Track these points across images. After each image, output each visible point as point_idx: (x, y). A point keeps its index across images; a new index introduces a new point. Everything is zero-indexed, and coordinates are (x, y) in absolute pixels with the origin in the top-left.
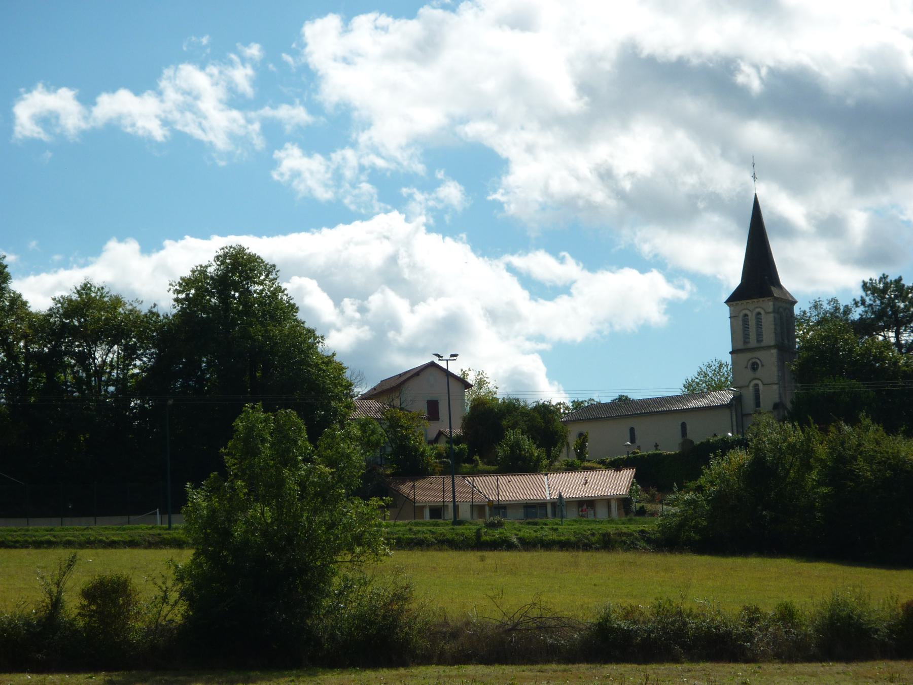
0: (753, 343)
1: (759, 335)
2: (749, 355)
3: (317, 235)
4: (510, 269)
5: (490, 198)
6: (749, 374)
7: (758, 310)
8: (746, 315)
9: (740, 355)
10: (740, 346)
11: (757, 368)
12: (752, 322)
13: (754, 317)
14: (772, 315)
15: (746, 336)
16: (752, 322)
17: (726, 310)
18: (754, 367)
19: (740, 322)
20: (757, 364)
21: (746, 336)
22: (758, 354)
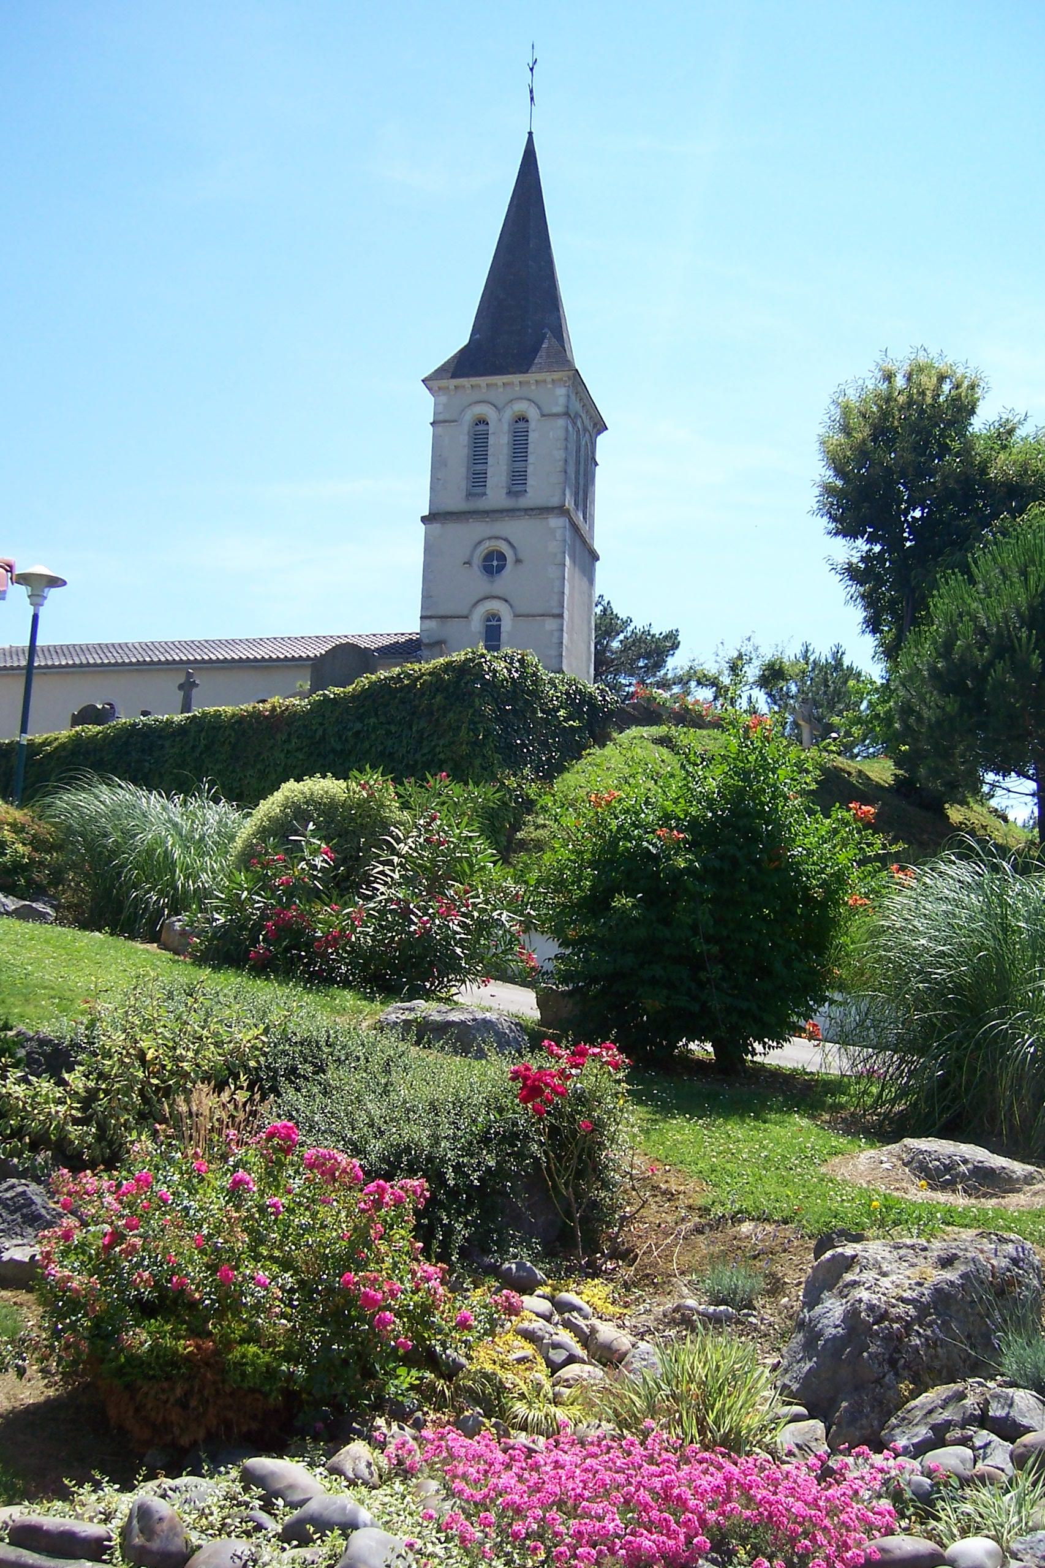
0: (496, 495)
1: (518, 480)
2: (478, 529)
3: (901, 361)
4: (538, 1296)
5: (93, 1472)
6: (476, 582)
7: (520, 407)
8: (482, 421)
9: (455, 530)
10: (456, 502)
11: (501, 568)
12: (499, 442)
13: (505, 427)
14: (561, 422)
15: (478, 480)
16: (499, 442)
17: (425, 404)
18: (494, 564)
19: (461, 438)
20: (502, 557)
21: (478, 480)
22: (511, 528)
